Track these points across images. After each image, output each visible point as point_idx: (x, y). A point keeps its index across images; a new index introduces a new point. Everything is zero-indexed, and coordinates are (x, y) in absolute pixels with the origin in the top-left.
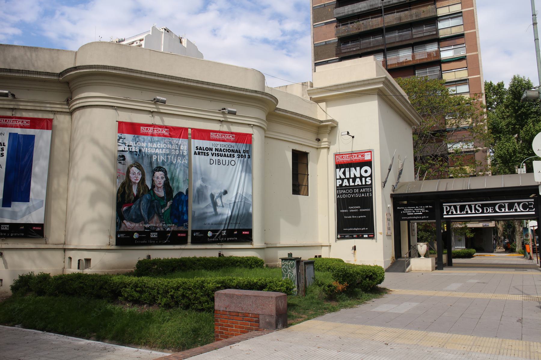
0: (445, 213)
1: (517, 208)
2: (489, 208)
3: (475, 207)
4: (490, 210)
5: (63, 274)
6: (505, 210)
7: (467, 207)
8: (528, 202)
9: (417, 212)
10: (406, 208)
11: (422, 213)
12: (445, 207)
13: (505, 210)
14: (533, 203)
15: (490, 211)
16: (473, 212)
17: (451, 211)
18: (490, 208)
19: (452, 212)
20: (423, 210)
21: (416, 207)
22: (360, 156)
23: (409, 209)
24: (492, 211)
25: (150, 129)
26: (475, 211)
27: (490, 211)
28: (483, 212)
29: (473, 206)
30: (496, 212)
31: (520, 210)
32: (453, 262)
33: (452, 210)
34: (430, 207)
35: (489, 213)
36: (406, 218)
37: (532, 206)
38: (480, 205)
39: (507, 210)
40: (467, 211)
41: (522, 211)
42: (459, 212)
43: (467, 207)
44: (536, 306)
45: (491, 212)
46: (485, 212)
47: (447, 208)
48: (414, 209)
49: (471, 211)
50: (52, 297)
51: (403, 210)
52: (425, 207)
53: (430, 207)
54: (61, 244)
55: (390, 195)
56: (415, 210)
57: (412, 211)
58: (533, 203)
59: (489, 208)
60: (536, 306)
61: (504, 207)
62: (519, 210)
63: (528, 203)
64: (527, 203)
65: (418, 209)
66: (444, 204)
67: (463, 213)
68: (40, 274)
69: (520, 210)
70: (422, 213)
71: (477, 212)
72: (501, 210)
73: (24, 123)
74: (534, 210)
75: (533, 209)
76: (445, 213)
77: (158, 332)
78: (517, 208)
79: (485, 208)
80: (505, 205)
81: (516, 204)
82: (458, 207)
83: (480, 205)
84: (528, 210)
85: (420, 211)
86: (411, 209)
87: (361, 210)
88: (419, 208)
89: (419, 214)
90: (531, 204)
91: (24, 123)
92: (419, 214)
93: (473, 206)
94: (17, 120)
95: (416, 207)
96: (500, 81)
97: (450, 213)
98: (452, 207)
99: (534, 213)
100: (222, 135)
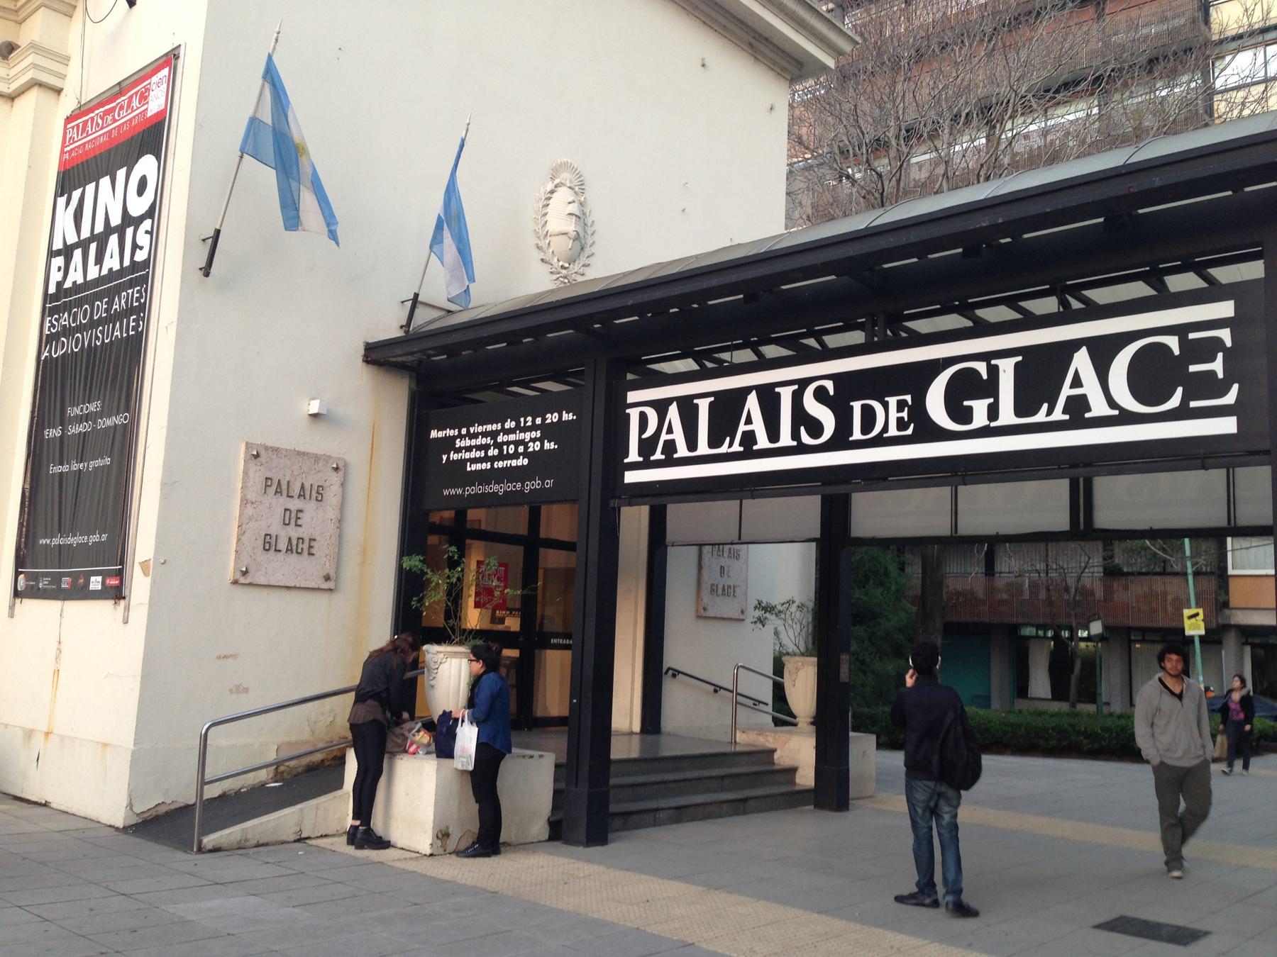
0: (634, 456)
2: (886, 406)
4: (889, 414)
6: (993, 412)
7: (752, 403)
8: (1180, 330)
9: (509, 457)
10: (510, 424)
11: (526, 462)
12: (634, 414)
13: (993, 412)
14: (1225, 335)
15: (885, 429)
16: (786, 440)
17: (664, 437)
18: (892, 401)
19: (670, 447)
20: (533, 440)
21: (507, 425)
23: (475, 436)
24: (901, 425)
25: (768, 396)
26: (795, 435)
27: (885, 429)
28: (841, 441)
29: (786, 394)
30: (927, 431)
31: (1112, 403)
33: (670, 431)
34: (565, 417)
35: (880, 441)
36: (460, 491)
37: (1217, 366)
38: (829, 385)
39: (1007, 416)
40: (673, 442)
41: (1126, 418)
42: (703, 448)
43: (752, 403)
44: (1206, 933)
45: (893, 431)
46: (857, 435)
47: (643, 419)
48: (493, 435)
49: (773, 434)
51: (448, 444)
52: (544, 419)
53: (565, 417)
54: (1254, 547)
55: (361, 351)
56: (500, 439)
57: (485, 447)
58: (1225, 335)
59: (886, 406)
60: (1206, 933)
61: (989, 388)
62: (1099, 408)
63: (1183, 342)
64: (1173, 342)
65: (512, 437)
66: (633, 397)
67: (1041, 417)
68: (311, 764)
69: (1112, 403)
70: (526, 462)
71: (806, 439)
73: (1078, 413)
74: (1230, 398)
75: (1223, 392)
76: (634, 456)
79: (857, 406)
80: (993, 371)
81: (1082, 361)
82: (704, 405)
83: (829, 385)
84: (1175, 401)
85: (521, 449)
86: (485, 434)
87: (455, 432)
88: (519, 428)
89: (514, 463)
90: (1208, 350)
92: (514, 463)
93: (786, 394)
94: (921, 375)
95: (507, 425)
97: (658, 455)
99: (1228, 425)
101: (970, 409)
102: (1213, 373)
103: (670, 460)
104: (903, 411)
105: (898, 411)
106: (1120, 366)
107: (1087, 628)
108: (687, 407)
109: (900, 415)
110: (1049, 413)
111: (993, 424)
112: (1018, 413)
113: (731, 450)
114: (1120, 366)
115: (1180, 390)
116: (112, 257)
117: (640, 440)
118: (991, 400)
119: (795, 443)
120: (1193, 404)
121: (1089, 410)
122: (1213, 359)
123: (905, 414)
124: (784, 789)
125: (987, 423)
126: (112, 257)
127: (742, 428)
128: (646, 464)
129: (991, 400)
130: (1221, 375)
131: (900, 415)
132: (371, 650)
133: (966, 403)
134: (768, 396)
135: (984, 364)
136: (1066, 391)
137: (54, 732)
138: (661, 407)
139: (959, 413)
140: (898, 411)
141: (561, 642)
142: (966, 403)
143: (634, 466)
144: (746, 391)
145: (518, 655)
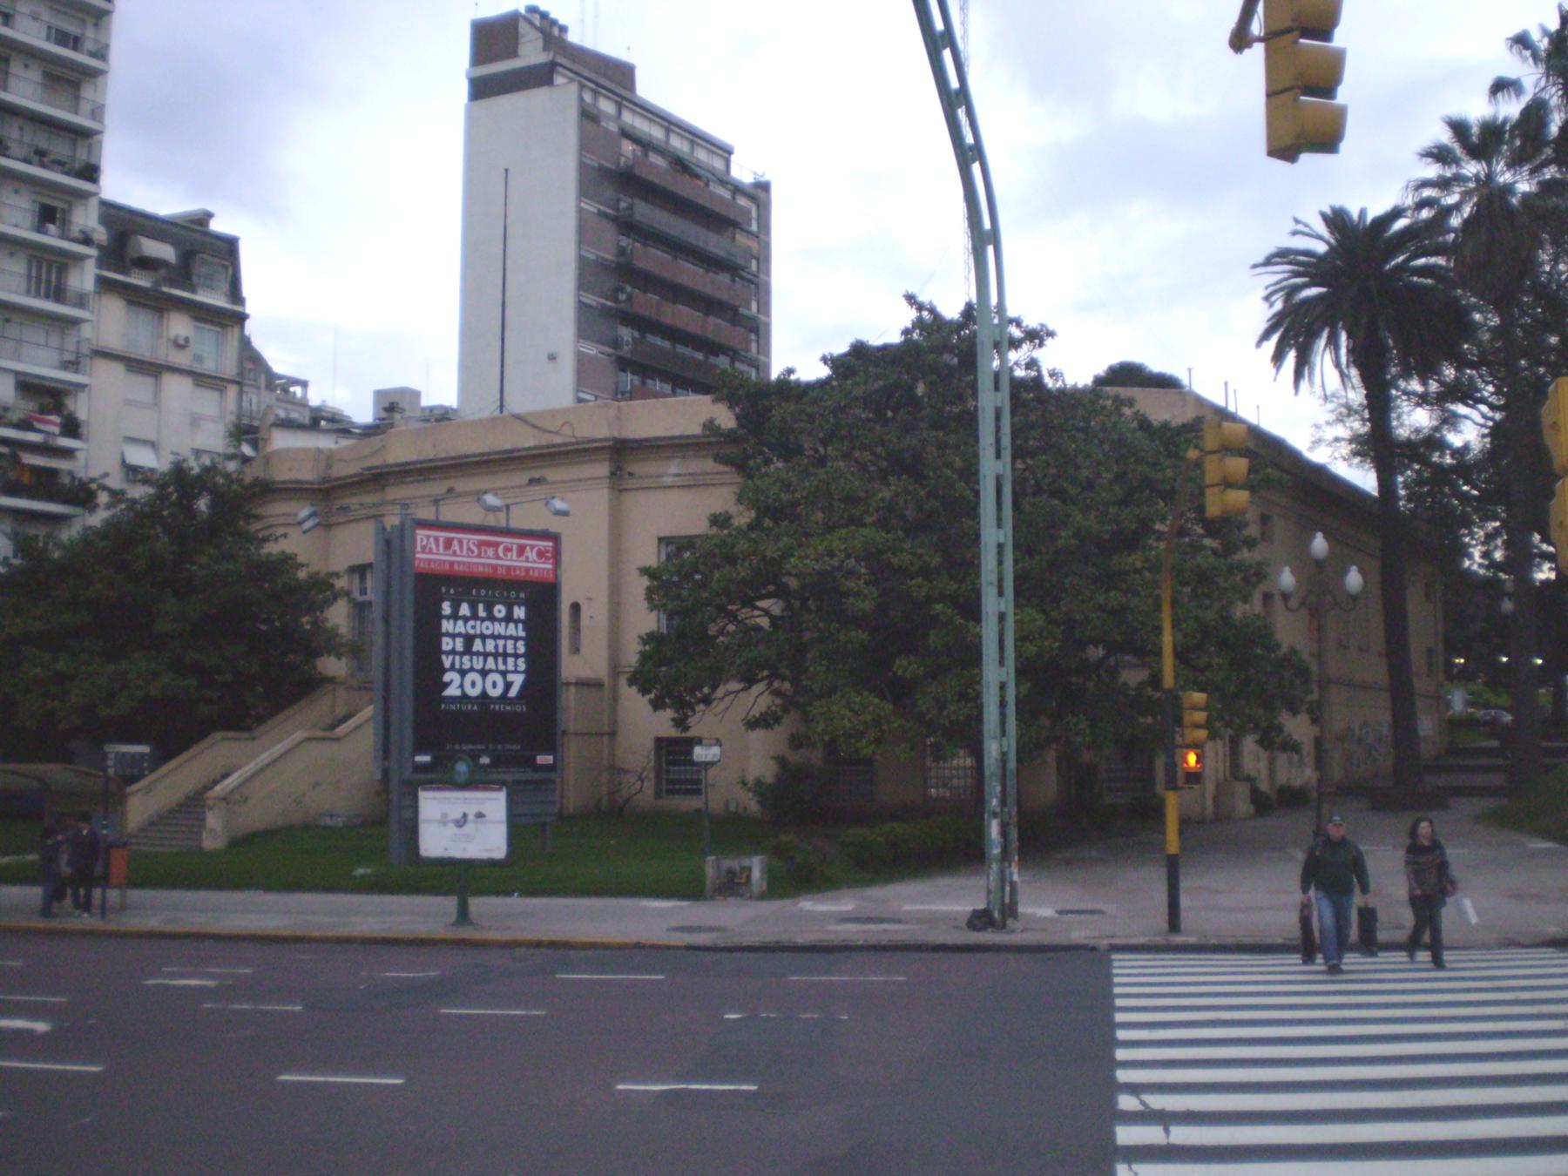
4: (491, 552)
12: (419, 538)
13: (512, 556)
16: (465, 553)
17: (429, 546)
22: (532, 555)
25: (460, 542)
28: (479, 556)
30: (498, 558)
32: (1445, 958)
35: (489, 558)
37: (549, 555)
39: (515, 557)
47: (422, 539)
50: (891, 381)
62: (531, 559)
71: (470, 554)
73: (527, 560)
76: (419, 549)
90: (548, 551)
91: (527, 560)
98: (432, 540)
100: (481, 544)
103: (431, 552)
106: (535, 550)
107: (1543, 263)
108: (436, 540)
114: (535, 550)
116: (1258, 407)
126: (1258, 407)
132: (643, 597)
134: (460, 542)
137: (630, 498)
138: (428, 537)
139: (505, 555)
141: (502, 707)
143: (419, 553)
145: (538, 757)
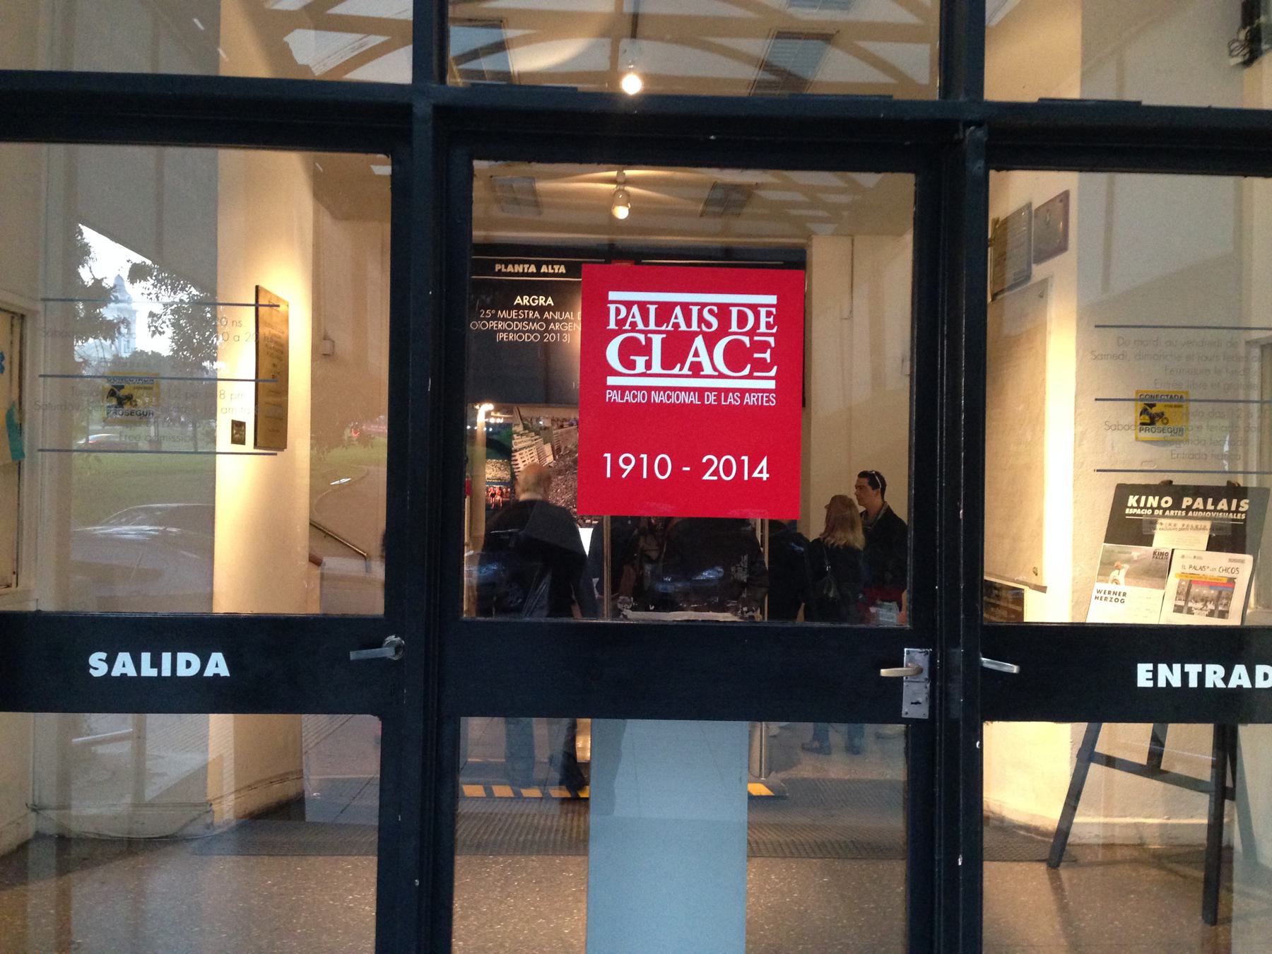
1: (704, 358)
3: (700, 312)
5: (852, 237)
6: (648, 365)
7: (678, 310)
12: (612, 308)
13: (648, 365)
17: (630, 319)
19: (633, 324)
24: (769, 326)
26: (699, 326)
29: (695, 309)
31: (715, 369)
33: (633, 317)
37: (767, 356)
38: (715, 309)
39: (657, 367)
41: (722, 376)
43: (678, 310)
47: (618, 311)
58: (771, 340)
61: (646, 350)
62: (708, 369)
63: (751, 341)
66: (613, 295)
67: (676, 371)
69: (715, 369)
72: (631, 365)
77: (780, 942)
78: (704, 358)
80: (649, 341)
82: (652, 309)
83: (715, 309)
84: (746, 371)
93: (695, 309)
96: (1067, 189)
97: (627, 327)
98: (635, 309)
101: (634, 362)
102: (765, 359)
104: (770, 317)
105: (767, 317)
109: (768, 320)
110: (681, 369)
111: (648, 372)
112: (663, 367)
113: (667, 329)
115: (749, 366)
117: (616, 320)
118: (647, 358)
119: (699, 330)
120: (756, 374)
121: (703, 371)
122: (765, 352)
123: (771, 320)
124: (1032, 261)
125: (644, 371)
127: (673, 320)
128: (754, 308)
129: (647, 358)
130: (769, 361)
131: (768, 320)
133: (632, 357)
135: (644, 335)
136: (690, 359)
138: (628, 305)
140: (767, 317)
142: (632, 357)
144: (675, 304)
